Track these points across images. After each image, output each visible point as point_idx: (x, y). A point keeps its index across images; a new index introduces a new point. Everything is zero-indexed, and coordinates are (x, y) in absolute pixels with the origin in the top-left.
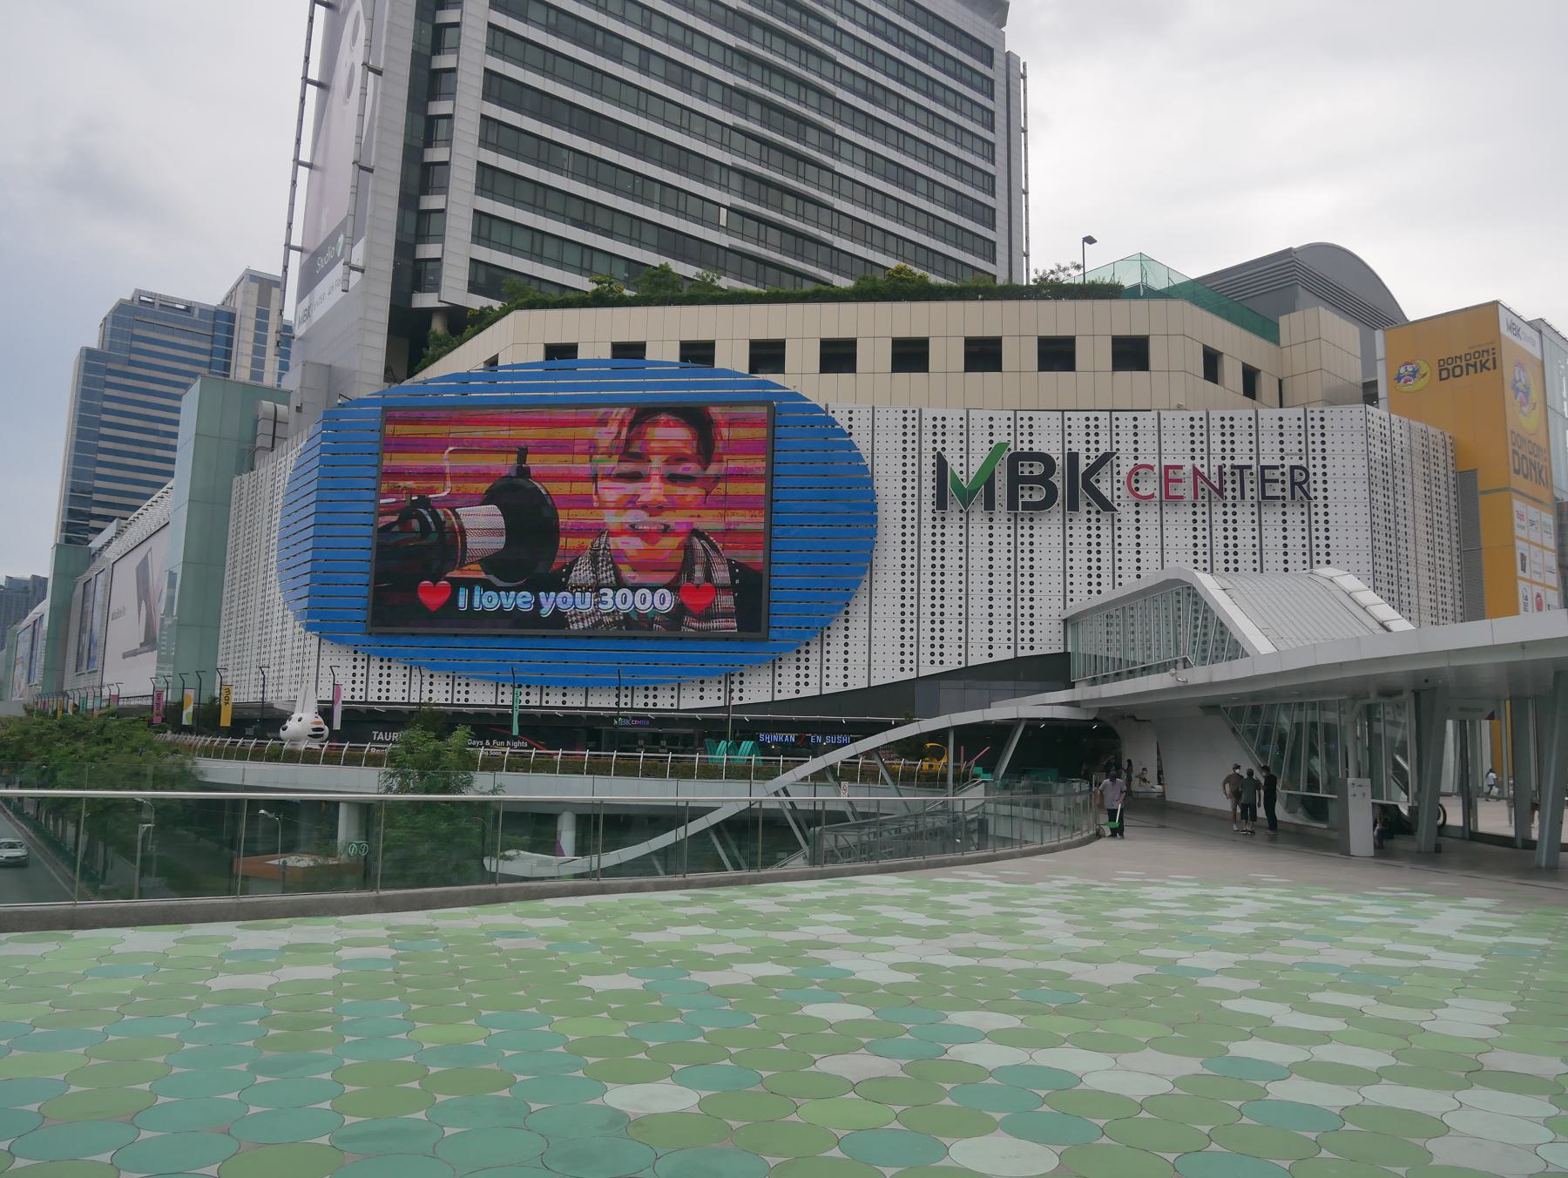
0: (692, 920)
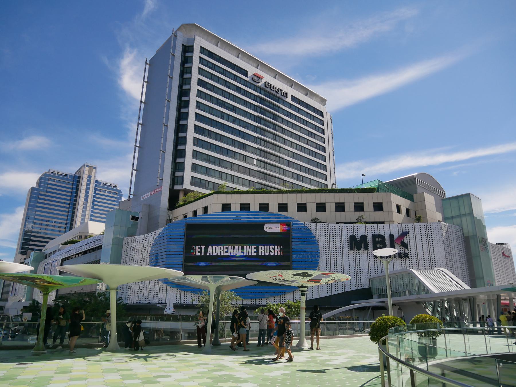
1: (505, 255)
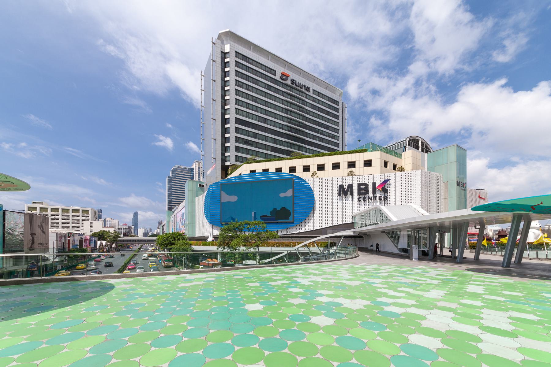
0: (273, 272)
1: (481, 198)
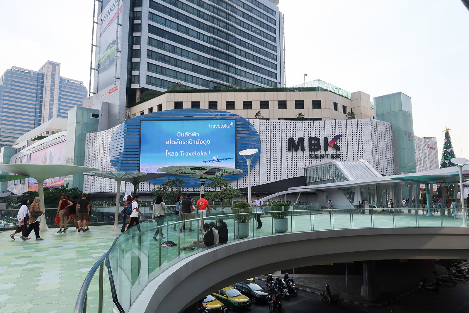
1: (430, 148)
